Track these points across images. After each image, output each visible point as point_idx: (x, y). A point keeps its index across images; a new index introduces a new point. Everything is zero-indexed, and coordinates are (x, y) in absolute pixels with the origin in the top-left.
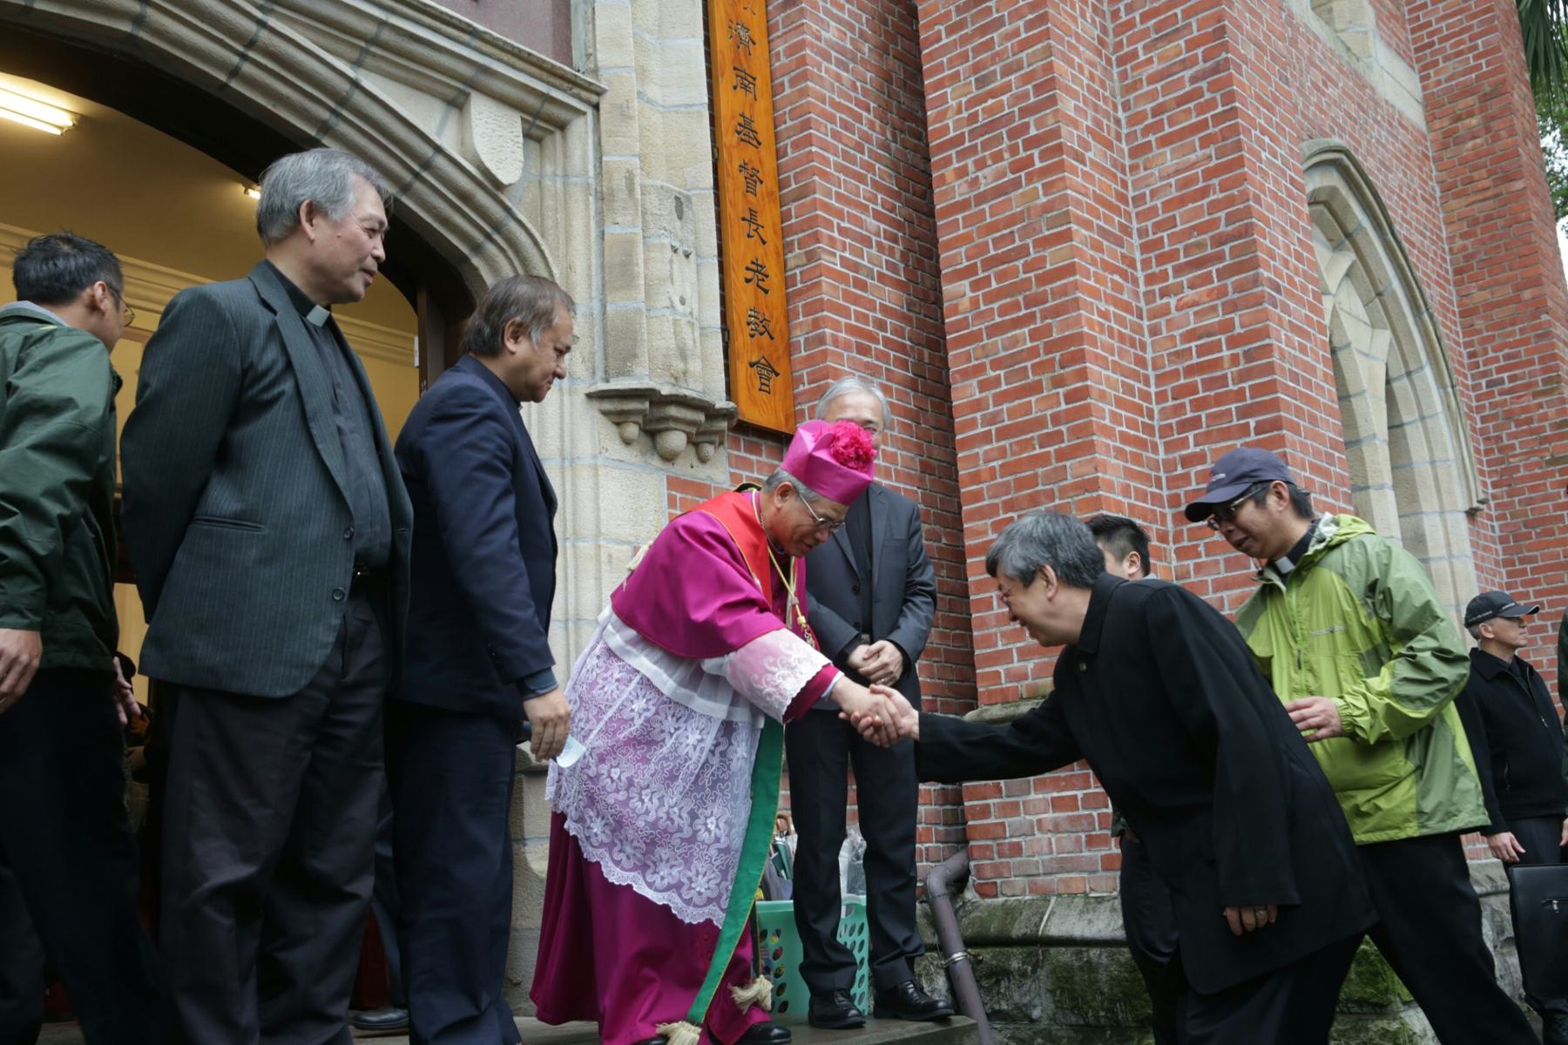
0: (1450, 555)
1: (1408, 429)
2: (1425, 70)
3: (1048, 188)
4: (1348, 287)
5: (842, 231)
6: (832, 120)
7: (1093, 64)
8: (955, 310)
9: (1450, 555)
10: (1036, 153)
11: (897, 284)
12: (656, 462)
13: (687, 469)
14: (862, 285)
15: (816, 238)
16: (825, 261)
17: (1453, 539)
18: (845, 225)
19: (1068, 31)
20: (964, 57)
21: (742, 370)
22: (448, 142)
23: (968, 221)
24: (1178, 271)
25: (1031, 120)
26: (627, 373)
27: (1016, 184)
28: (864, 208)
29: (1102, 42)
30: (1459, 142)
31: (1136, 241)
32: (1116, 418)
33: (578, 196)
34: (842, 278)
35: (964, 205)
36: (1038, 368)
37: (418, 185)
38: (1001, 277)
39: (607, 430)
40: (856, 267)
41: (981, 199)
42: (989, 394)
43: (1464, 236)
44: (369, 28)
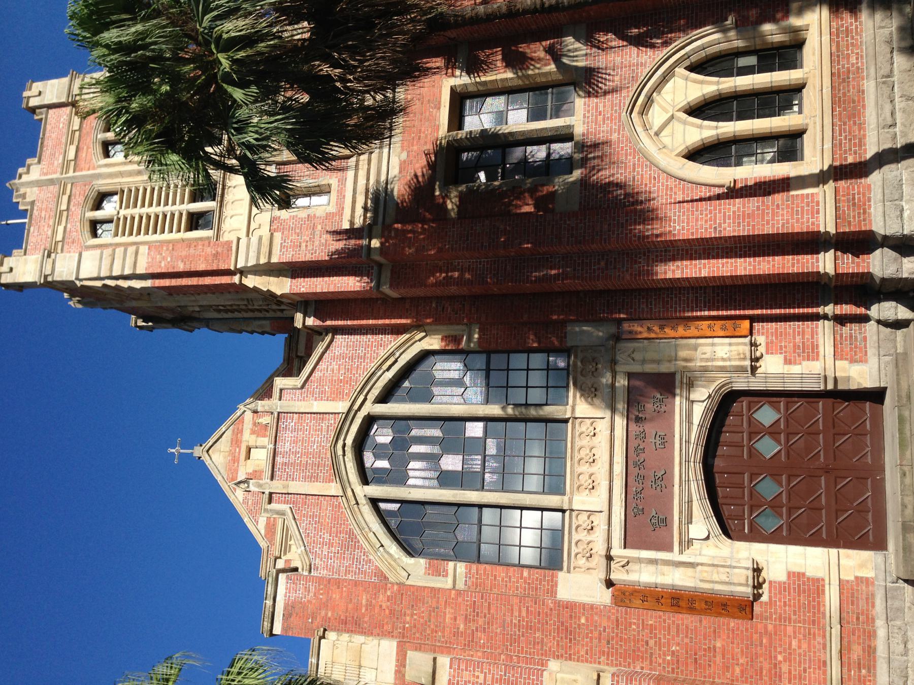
21: (737, 334)
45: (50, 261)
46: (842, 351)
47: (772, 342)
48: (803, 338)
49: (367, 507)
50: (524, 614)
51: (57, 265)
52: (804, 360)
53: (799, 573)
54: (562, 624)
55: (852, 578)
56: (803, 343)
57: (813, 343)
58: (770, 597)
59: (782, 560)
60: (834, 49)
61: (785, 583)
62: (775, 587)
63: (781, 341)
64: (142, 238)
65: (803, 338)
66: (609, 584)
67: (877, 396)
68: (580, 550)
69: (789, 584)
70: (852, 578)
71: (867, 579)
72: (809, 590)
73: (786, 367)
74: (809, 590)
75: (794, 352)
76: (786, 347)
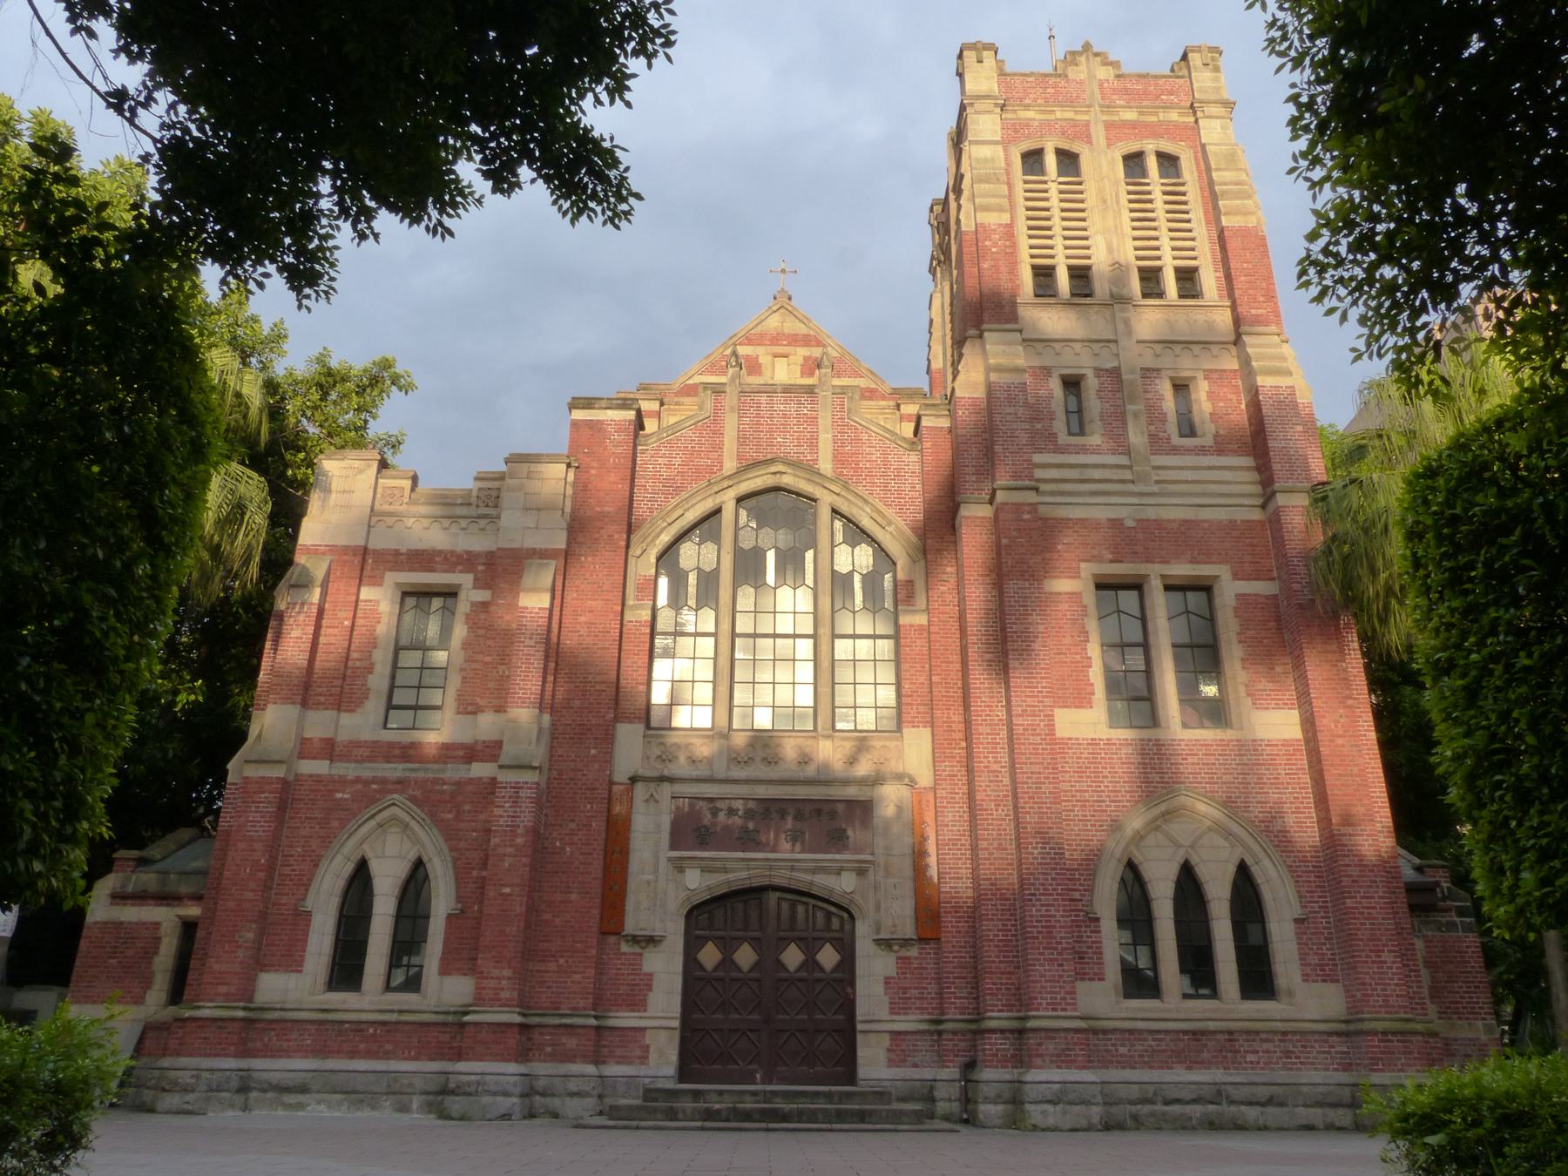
45: (992, 107)
51: (986, 117)
59: (665, 970)
60: (1263, 1036)
64: (1022, 214)
66: (634, 780)
67: (851, 1077)
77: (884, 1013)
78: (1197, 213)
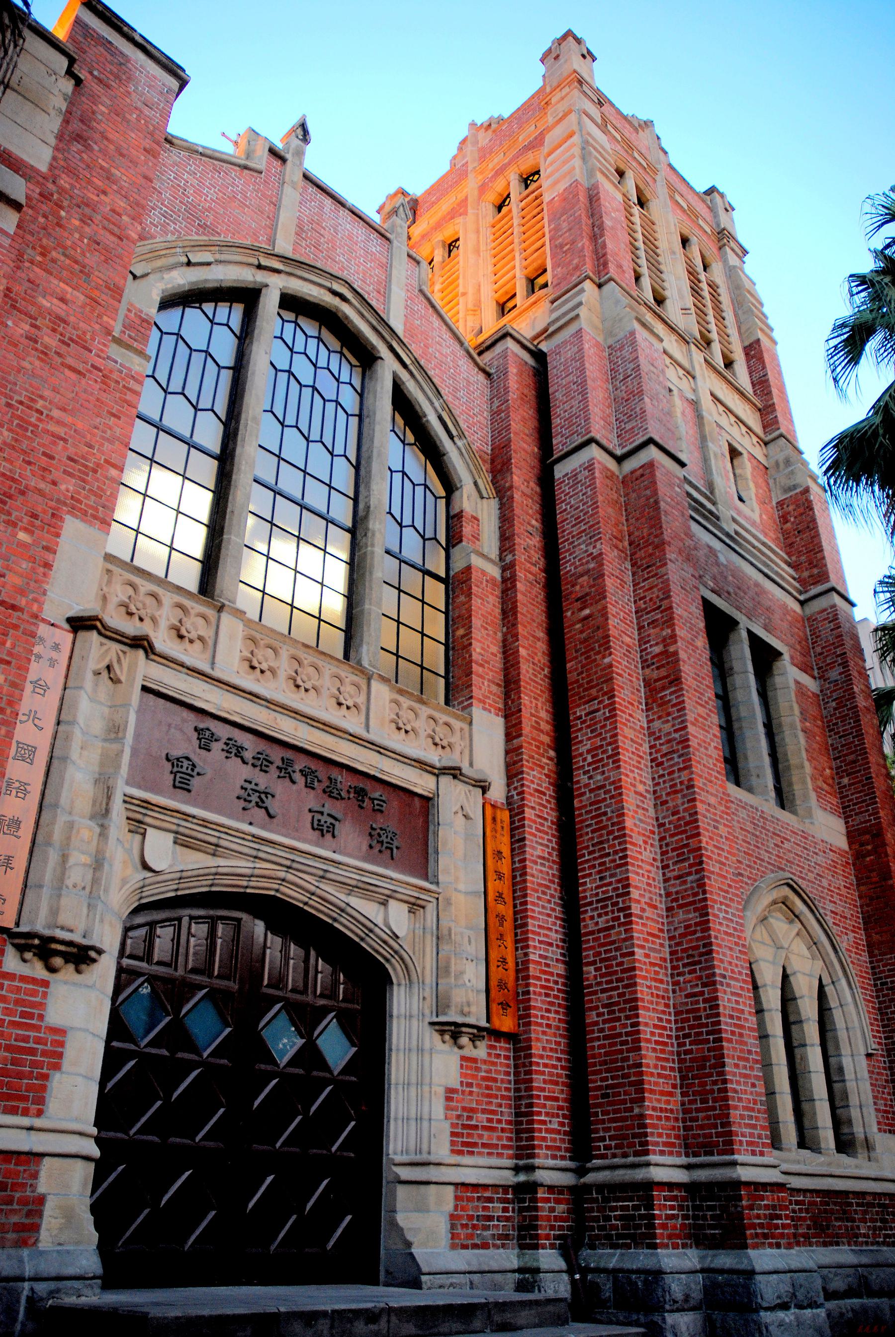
0: (857, 1079)
1: (834, 1011)
2: (847, 818)
3: (626, 931)
4: (798, 940)
5: (540, 942)
6: (537, 891)
7: (649, 871)
8: (588, 979)
9: (857, 1079)
10: (622, 914)
11: (564, 962)
12: (456, 1049)
13: (469, 1051)
14: (547, 965)
15: (527, 947)
16: (532, 957)
17: (858, 1069)
18: (541, 939)
19: (637, 859)
20: (594, 866)
21: (494, 1007)
22: (379, 921)
23: (594, 940)
24: (684, 965)
25: (620, 900)
26: (445, 1014)
27: (613, 927)
28: (550, 929)
29: (654, 859)
30: (865, 856)
31: (667, 950)
32: (653, 1034)
33: (428, 937)
34: (539, 963)
35: (592, 933)
36: (620, 1011)
37: (368, 939)
38: (606, 967)
39: (437, 1037)
40: (546, 957)
41: (600, 931)
42: (600, 1019)
43: (868, 905)
44: (354, 883)
46: (470, 1199)
47: (478, 1069)
48: (485, 1128)
49: (251, 278)
50: (52, 427)
52: (453, 1125)
53: (60, 1055)
54: (23, 493)
55: (42, 1189)
56: (476, 1127)
57: (475, 1145)
58: (11, 976)
61: (41, 1017)
62: (34, 993)
63: (478, 1086)
65: (485, 1128)
68: (141, 597)
69: (37, 1028)
70: (42, 1189)
71: (36, 1228)
72: (20, 1075)
73: (441, 1091)
74: (20, 1075)
75: (464, 1109)
76: (471, 1093)
77: (442, 1150)
78: (168, 251)
